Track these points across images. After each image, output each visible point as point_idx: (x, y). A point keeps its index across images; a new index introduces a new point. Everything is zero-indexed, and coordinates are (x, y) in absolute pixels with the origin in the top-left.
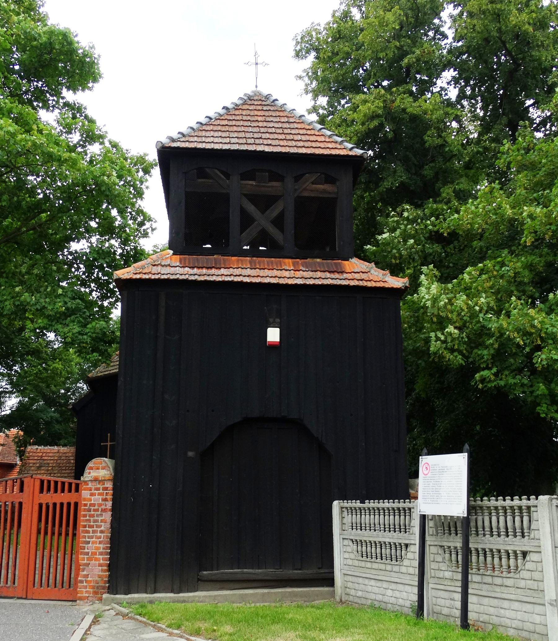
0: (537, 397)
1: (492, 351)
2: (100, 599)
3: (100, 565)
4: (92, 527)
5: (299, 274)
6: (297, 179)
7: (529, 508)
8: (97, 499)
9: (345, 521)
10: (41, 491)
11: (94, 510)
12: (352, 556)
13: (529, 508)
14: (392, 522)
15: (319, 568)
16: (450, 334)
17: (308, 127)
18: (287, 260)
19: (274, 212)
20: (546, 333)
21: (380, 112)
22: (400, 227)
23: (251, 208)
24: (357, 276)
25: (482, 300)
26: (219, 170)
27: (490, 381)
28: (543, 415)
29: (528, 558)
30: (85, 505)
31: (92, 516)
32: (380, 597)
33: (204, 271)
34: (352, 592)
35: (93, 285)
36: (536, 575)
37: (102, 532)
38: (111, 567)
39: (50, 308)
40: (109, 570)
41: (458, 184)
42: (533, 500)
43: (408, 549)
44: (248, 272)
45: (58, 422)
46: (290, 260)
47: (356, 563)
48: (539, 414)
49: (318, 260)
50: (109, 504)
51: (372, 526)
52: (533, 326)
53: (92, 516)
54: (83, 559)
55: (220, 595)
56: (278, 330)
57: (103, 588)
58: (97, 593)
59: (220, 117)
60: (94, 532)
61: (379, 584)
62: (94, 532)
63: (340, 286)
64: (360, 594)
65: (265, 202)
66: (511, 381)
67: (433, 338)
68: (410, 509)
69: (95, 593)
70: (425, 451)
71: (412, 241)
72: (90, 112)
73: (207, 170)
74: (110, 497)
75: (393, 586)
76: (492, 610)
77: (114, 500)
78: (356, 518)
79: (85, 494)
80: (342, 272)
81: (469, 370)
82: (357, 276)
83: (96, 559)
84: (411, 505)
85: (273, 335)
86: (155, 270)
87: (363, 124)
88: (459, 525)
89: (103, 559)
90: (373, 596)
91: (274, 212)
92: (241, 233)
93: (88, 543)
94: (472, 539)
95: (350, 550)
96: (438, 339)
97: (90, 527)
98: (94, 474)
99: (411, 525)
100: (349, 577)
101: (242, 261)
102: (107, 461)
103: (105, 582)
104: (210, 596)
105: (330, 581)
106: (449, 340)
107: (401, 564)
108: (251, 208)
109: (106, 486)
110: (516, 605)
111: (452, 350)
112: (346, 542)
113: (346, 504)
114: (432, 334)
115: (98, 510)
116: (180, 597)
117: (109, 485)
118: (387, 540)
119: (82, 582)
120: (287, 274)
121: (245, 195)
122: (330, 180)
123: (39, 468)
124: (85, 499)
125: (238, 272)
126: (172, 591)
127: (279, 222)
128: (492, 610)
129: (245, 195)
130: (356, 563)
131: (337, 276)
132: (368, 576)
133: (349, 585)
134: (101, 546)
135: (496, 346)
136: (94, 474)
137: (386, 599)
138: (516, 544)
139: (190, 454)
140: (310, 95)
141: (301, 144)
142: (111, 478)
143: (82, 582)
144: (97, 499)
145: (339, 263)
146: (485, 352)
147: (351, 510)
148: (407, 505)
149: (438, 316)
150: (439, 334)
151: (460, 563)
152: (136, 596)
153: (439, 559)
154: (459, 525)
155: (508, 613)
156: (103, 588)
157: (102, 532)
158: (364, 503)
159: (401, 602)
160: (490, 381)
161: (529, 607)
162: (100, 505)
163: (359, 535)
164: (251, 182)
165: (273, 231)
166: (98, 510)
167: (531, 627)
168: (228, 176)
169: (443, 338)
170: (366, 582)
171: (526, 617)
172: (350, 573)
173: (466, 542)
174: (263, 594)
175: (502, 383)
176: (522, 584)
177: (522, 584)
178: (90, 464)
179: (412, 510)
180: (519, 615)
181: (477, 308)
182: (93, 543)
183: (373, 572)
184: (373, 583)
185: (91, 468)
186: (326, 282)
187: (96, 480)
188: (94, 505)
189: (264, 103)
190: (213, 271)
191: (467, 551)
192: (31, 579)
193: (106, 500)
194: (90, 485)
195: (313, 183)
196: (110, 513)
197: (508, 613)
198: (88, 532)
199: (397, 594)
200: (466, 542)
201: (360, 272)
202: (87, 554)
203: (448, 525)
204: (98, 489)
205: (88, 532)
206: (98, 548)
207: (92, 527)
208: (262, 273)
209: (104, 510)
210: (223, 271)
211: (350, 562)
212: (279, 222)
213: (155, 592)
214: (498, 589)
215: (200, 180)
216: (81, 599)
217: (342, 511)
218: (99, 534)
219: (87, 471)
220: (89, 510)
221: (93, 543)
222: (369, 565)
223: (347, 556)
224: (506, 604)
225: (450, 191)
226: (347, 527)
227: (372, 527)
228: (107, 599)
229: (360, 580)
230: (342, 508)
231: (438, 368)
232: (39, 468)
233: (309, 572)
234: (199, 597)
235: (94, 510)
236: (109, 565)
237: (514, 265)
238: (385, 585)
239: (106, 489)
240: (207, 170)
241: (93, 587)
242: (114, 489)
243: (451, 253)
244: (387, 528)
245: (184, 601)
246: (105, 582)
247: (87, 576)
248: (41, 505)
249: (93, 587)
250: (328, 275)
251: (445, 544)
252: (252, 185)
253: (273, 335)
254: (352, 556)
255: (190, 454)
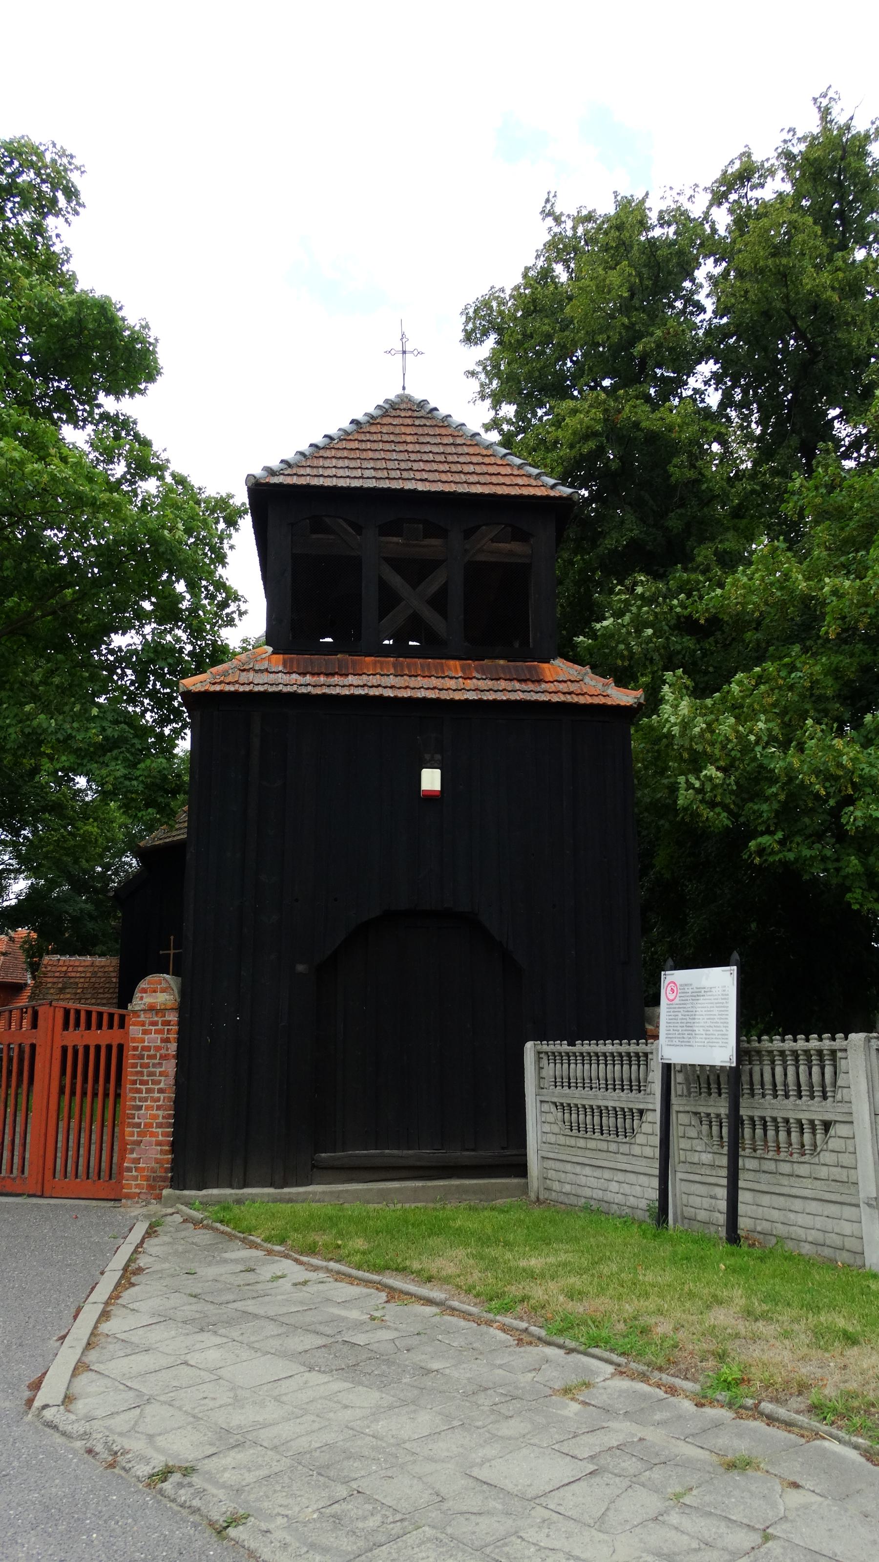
0: (846, 877)
1: (775, 806)
2: (159, 1197)
3: (159, 1144)
4: (146, 1083)
5: (470, 684)
6: (468, 533)
7: (833, 1052)
8: (153, 1039)
9: (544, 1073)
10: (66, 1026)
11: (149, 1057)
12: (556, 1129)
13: (833, 1052)
14: (617, 1075)
15: (503, 1148)
16: (710, 779)
17: (485, 452)
18: (452, 663)
19: (432, 585)
20: (860, 776)
21: (599, 428)
22: (629, 610)
23: (396, 581)
24: (562, 687)
25: (761, 725)
26: (345, 520)
27: (773, 853)
28: (856, 907)
29: (832, 1132)
30: (135, 1049)
31: (147, 1066)
32: (598, 1194)
33: (322, 679)
34: (556, 1186)
35: (146, 701)
36: (845, 1159)
37: (161, 1091)
38: (175, 1147)
39: (79, 737)
40: (173, 1151)
41: (721, 542)
42: (839, 1042)
43: (644, 1118)
44: (391, 680)
45: (91, 917)
46: (458, 663)
47: (562, 1140)
48: (849, 904)
49: (502, 662)
50: (173, 1047)
51: (587, 1081)
52: (840, 765)
53: (147, 1066)
54: (131, 1134)
55: (347, 1191)
56: (438, 772)
57: (164, 1179)
58: (153, 1188)
59: (346, 436)
60: (149, 1091)
61: (598, 1173)
62: (149, 1091)
63: (536, 702)
64: (567, 1188)
65: (417, 570)
66: (806, 853)
67: (683, 785)
68: (646, 1055)
69: (151, 1187)
70: (670, 962)
71: (650, 631)
72: (143, 429)
73: (327, 520)
74: (173, 1036)
75: (620, 1176)
76: (775, 1215)
77: (179, 1041)
78: (561, 1069)
79: (134, 1031)
80: (539, 681)
81: (737, 836)
82: (562, 687)
83: (152, 1135)
84: (648, 1049)
85: (431, 780)
86: (244, 677)
87: (572, 446)
88: (723, 1079)
89: (162, 1134)
90: (588, 1192)
91: (432, 585)
92: (381, 618)
93: (140, 1108)
94: (744, 1102)
95: (552, 1120)
96: (690, 786)
97: (143, 1083)
98: (148, 999)
99: (649, 1079)
100: (550, 1162)
101: (381, 663)
102: (168, 979)
103: (166, 1170)
104: (331, 1193)
105: (520, 1169)
106: (708, 787)
107: (633, 1141)
108: (396, 581)
109: (167, 1018)
110: (813, 1206)
111: (712, 805)
112: (545, 1107)
113: (545, 1047)
114: (682, 779)
115: (153, 1057)
116: (285, 1194)
117: (173, 1017)
118: (610, 1104)
119: (129, 1170)
120: (452, 684)
121: (386, 559)
122: (520, 536)
123: (61, 990)
124: (134, 1040)
125: (374, 680)
126: (272, 1185)
127: (439, 602)
128: (775, 1215)
129: (386, 559)
130: (562, 1140)
131: (530, 686)
132: (580, 1160)
133: (551, 1174)
134: (160, 1113)
135: (782, 797)
136: (148, 999)
137: (609, 1197)
138: (813, 1110)
139: (300, 968)
140: (488, 401)
141: (473, 479)
142: (176, 1005)
143: (129, 1170)
144: (153, 1039)
145: (534, 666)
146: (765, 807)
147: (554, 1056)
148: (642, 1048)
149: (691, 750)
150: (692, 779)
151: (725, 1139)
152: (215, 1191)
153: (693, 1133)
154: (723, 1079)
155: (801, 1219)
156: (164, 1179)
157: (161, 1091)
158: (575, 1045)
159: (632, 1201)
160: (773, 853)
161: (833, 1209)
162: (158, 1049)
163: (566, 1096)
164: (395, 539)
165: (429, 615)
166: (153, 1057)
167: (837, 1241)
168: (359, 529)
169: (697, 784)
170: (578, 1169)
171: (830, 1224)
172: (551, 1155)
173: (735, 1107)
174: (415, 1190)
175: (791, 856)
176: (823, 1172)
177: (823, 1172)
178: (143, 984)
179: (650, 1056)
180: (819, 1222)
181: (752, 738)
182: (147, 1108)
183: (589, 1154)
184: (588, 1171)
185: (144, 991)
186: (513, 696)
187: (151, 1009)
188: (148, 1049)
189: (416, 414)
190: (336, 679)
191: (736, 1121)
192: (49, 1164)
193: (166, 1040)
194: (142, 1018)
195: (492, 540)
196: (174, 1062)
197: (801, 1219)
198: (139, 1091)
199: (626, 1188)
200: (735, 1107)
201: (566, 681)
202: (138, 1125)
203: (705, 1079)
204: (154, 1024)
205: (139, 1091)
206: (155, 1117)
207: (146, 1083)
208: (413, 682)
209: (164, 1057)
210: (351, 679)
211: (552, 1138)
212: (439, 602)
213: (245, 1186)
214: (785, 1181)
215: (314, 536)
216: (128, 1196)
217: (540, 1058)
218: (156, 1095)
219: (137, 995)
220: (141, 1057)
221: (147, 1108)
222: (581, 1143)
223: (547, 1128)
224: (798, 1204)
225: (709, 552)
226: (548, 1083)
227: (587, 1083)
228: (169, 1197)
229: (569, 1167)
230: (539, 1053)
231: (690, 832)
232: (61, 990)
233: (484, 1155)
234: (314, 1193)
235: (149, 1057)
236: (173, 1144)
237: (810, 669)
238: (607, 1174)
239: (168, 1023)
240: (327, 520)
241: (148, 1179)
242: (180, 1023)
243: (710, 651)
244: (611, 1085)
245: (290, 1201)
246: (166, 1170)
247: (137, 1161)
248: (64, 1049)
249: (148, 1179)
250: (517, 685)
251: (702, 1110)
252: (398, 543)
253: (431, 780)
254: (556, 1129)
255: (300, 968)
